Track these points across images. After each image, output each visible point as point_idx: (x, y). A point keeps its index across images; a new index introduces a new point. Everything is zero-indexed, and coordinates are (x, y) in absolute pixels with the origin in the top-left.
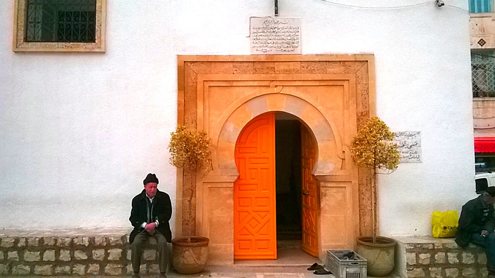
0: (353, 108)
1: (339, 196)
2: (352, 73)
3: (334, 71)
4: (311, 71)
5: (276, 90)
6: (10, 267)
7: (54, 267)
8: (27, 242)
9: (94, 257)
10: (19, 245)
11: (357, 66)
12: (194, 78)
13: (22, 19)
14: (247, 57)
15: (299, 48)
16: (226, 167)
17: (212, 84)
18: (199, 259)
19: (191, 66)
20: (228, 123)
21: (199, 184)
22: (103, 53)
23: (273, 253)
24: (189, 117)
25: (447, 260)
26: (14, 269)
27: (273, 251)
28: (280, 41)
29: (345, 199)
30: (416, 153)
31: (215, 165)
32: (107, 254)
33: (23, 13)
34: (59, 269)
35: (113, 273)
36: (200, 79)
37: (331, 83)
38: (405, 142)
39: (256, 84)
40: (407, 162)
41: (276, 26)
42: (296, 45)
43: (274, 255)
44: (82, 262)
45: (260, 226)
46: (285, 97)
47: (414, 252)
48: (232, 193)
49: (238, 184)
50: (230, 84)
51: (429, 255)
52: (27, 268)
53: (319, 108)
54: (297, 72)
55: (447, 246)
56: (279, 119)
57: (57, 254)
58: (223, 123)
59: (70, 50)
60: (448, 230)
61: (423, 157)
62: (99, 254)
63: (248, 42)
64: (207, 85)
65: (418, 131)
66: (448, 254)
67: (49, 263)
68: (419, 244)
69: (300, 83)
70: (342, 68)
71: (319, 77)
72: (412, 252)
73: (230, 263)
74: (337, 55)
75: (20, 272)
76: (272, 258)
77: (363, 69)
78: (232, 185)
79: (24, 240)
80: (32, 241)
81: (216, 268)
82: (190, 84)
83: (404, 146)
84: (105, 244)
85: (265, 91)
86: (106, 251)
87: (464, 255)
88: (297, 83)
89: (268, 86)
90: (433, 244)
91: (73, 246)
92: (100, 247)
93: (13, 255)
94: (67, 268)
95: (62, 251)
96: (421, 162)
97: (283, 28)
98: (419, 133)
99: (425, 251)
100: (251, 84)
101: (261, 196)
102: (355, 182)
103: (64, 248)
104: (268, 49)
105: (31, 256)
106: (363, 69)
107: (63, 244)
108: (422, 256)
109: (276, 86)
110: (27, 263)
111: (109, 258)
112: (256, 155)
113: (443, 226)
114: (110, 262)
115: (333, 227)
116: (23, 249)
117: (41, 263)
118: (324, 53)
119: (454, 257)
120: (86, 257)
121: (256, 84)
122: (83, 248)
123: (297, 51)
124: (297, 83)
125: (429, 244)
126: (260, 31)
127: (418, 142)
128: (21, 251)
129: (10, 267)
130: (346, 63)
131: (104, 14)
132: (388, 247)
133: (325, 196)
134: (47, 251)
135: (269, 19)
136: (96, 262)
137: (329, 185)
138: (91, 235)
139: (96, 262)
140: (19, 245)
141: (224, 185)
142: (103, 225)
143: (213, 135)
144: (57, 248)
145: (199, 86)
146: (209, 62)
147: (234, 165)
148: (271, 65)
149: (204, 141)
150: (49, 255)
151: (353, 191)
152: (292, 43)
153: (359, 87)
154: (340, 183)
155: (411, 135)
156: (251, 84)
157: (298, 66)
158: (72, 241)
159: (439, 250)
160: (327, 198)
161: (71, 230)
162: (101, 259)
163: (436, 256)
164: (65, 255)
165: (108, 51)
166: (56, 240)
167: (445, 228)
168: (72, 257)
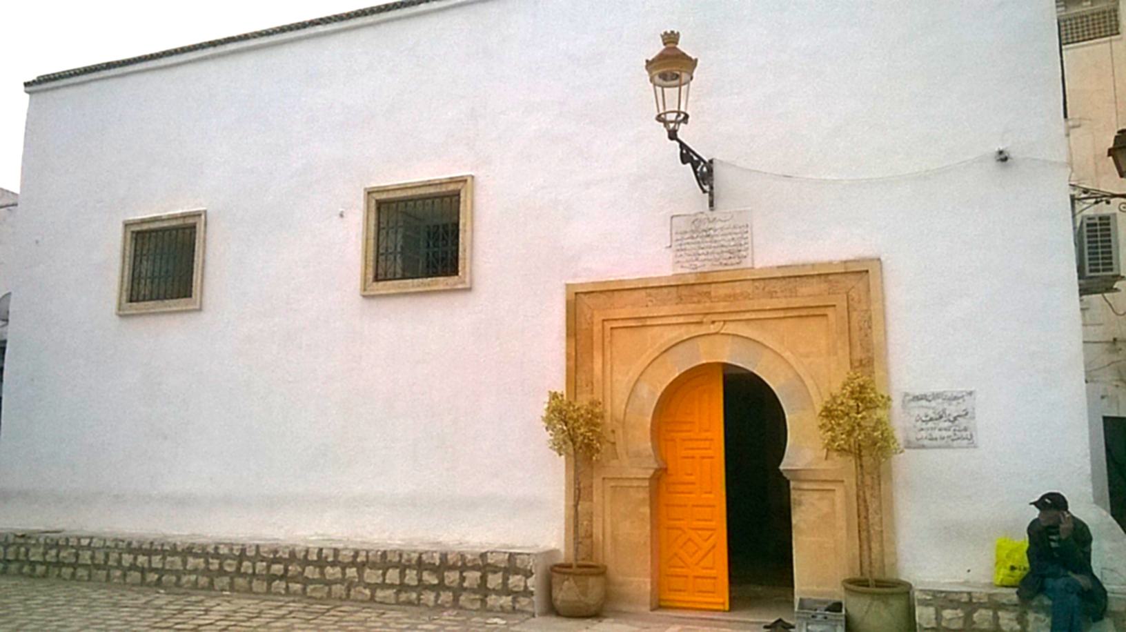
0: (843, 353)
1: (824, 506)
2: (844, 296)
3: (808, 293)
4: (771, 295)
5: (713, 328)
6: (349, 590)
7: (398, 592)
8: (367, 556)
9: (446, 582)
10: (359, 560)
11: (851, 281)
12: (590, 315)
13: (373, 222)
14: (667, 278)
15: (749, 260)
16: (638, 455)
17: (615, 324)
18: (584, 594)
19: (585, 298)
20: (639, 385)
21: (597, 482)
22: (469, 289)
23: (721, 600)
24: (582, 377)
25: (998, 625)
26: (352, 593)
27: (723, 597)
28: (719, 250)
29: (834, 512)
30: (965, 429)
31: (620, 449)
32: (463, 579)
33: (372, 242)
34: (403, 597)
35: (469, 606)
36: (598, 318)
37: (804, 313)
38: (944, 410)
39: (681, 320)
40: (949, 447)
41: (711, 226)
42: (744, 253)
43: (723, 604)
44: (432, 587)
45: (701, 553)
46: (730, 339)
47: (931, 605)
48: (647, 496)
49: (659, 478)
50: (641, 323)
51: (960, 613)
52: (367, 592)
53: (787, 354)
54: (747, 296)
55: (997, 598)
56: (729, 372)
57: (402, 575)
58: (633, 384)
59: (428, 288)
60: (1017, 572)
61: (980, 438)
62: (452, 577)
63: (670, 256)
64: (608, 325)
65: (969, 390)
66: (1000, 613)
67: (392, 586)
68: (942, 592)
69: (753, 316)
70: (824, 286)
71: (783, 303)
72: (927, 605)
73: (646, 609)
74: (813, 265)
75: (360, 597)
76: (721, 607)
77: (861, 285)
78: (647, 483)
79: (364, 553)
80: (375, 555)
81: (618, 614)
82: (585, 326)
83: (941, 417)
84: (460, 564)
85: (695, 331)
86: (461, 573)
87: (1031, 616)
88: (747, 316)
89: (700, 323)
90: (969, 593)
91: (420, 565)
92: (453, 568)
93: (351, 572)
94: (414, 596)
95: (407, 572)
96: (975, 447)
97: (722, 229)
98: (970, 393)
99: (955, 604)
100: (674, 320)
101: (701, 503)
102: (851, 481)
103: (409, 567)
104: (698, 264)
105: (372, 576)
106: (861, 285)
107: (409, 560)
108: (948, 614)
109: (713, 322)
110: (368, 585)
111: (465, 585)
112: (692, 435)
113: (1010, 564)
114: (465, 589)
115: (819, 556)
116: (364, 564)
117: (384, 586)
118: (789, 263)
119: (1011, 620)
120: (436, 582)
121: (681, 320)
122: (434, 569)
123: (747, 263)
124: (747, 316)
125: (962, 592)
126: (687, 236)
127: (970, 410)
128: (361, 567)
129: (349, 590)
130: (831, 278)
131: (468, 234)
132: (886, 594)
133: (800, 504)
134: (391, 571)
135: (700, 216)
136: (448, 588)
137: (805, 486)
138: (444, 550)
139: (448, 588)
140: (359, 560)
141: (635, 483)
142: (468, 538)
143: (615, 405)
144: (403, 568)
145: (597, 328)
146: (610, 291)
147: (651, 451)
148: (705, 289)
149: (595, 416)
150: (393, 576)
151: (847, 496)
152: (736, 252)
153: (854, 315)
154: (825, 484)
155: (956, 398)
156: (674, 320)
157: (748, 288)
158: (420, 558)
159: (981, 605)
160: (803, 508)
161: (423, 543)
162: (455, 584)
163: (975, 615)
164: (411, 577)
165: (476, 286)
166: (401, 555)
167: (1013, 568)
168: (420, 580)
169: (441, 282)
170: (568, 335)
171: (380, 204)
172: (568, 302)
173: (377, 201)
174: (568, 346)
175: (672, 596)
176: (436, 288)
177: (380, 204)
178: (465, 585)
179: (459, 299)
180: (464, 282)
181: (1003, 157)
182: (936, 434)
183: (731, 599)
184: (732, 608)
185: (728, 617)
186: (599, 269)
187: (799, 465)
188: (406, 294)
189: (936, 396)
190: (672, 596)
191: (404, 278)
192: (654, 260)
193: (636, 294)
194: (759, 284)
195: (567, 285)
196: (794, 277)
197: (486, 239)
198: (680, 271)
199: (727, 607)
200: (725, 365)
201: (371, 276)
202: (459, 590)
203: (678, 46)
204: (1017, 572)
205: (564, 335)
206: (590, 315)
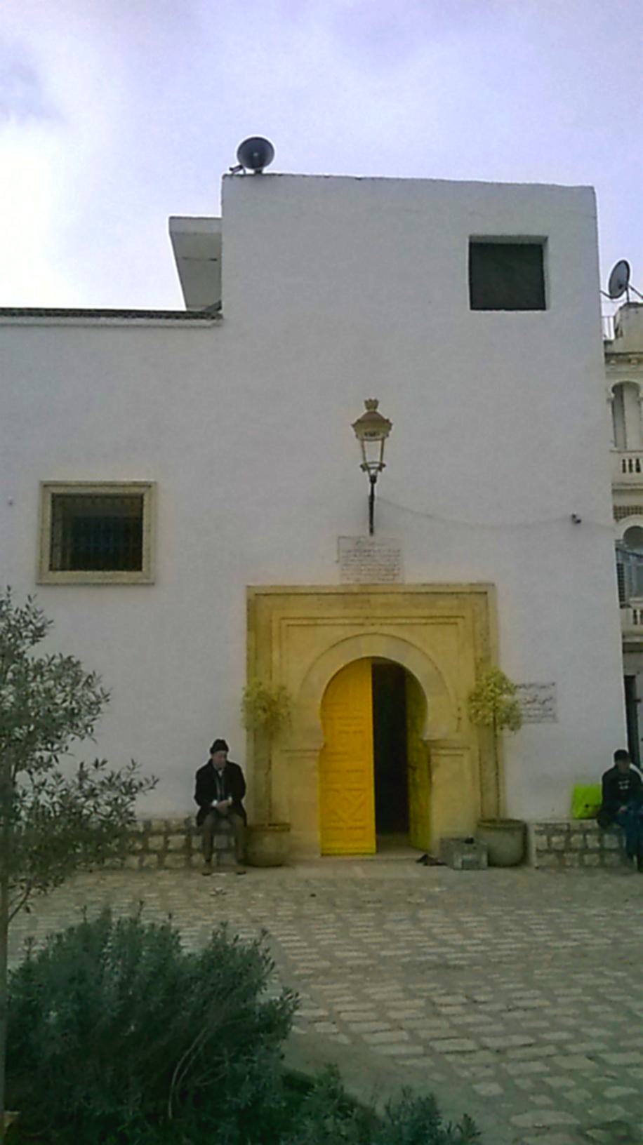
3: (445, 606)
12: (265, 613)
17: (292, 622)
22: (153, 584)
27: (370, 843)
32: (167, 842)
50: (312, 623)
51: (562, 838)
60: (590, 809)
64: (285, 622)
71: (426, 612)
73: (318, 856)
88: (399, 621)
89: (362, 625)
92: (158, 833)
100: (341, 621)
108: (554, 839)
114: (170, 851)
123: (399, 580)
124: (399, 621)
137: (443, 752)
138: (147, 817)
145: (275, 625)
159: (575, 832)
169: (125, 576)
170: (249, 630)
171: (55, 497)
172: (249, 601)
173: (53, 495)
174: (248, 638)
175: (334, 845)
176: (118, 581)
177: (55, 497)
178: (171, 847)
179: (142, 592)
180: (148, 578)
181: (576, 521)
182: (531, 713)
183: (378, 843)
184: (381, 846)
185: (375, 857)
186: (276, 575)
187: (436, 735)
188: (87, 584)
189: (531, 685)
190: (334, 845)
191: (63, 569)
192: (323, 571)
193: (309, 597)
194: (407, 596)
195: (249, 587)
196: (435, 593)
197: (165, 536)
198: (345, 581)
199: (374, 850)
200: (373, 658)
201: (46, 565)
202: (164, 852)
203: (378, 410)
204: (590, 809)
205: (245, 626)
206: (265, 613)
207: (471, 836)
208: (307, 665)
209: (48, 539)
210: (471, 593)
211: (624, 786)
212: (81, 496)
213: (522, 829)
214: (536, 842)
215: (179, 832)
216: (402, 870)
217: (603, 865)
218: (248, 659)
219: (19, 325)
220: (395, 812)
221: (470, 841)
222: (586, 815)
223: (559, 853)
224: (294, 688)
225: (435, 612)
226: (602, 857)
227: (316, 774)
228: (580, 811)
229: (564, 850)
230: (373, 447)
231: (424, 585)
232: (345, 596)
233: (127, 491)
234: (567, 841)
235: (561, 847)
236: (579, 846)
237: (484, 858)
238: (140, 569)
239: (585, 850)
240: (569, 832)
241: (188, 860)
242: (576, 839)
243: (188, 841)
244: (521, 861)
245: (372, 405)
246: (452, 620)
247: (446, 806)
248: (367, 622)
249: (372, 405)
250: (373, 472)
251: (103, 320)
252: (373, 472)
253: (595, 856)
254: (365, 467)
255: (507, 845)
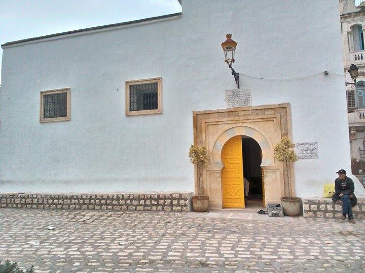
17: (209, 124)
22: (161, 113)
32: (165, 202)
50: (217, 124)
51: (316, 206)
60: (331, 194)
64: (207, 124)
73: (221, 209)
88: (250, 121)
92: (162, 199)
108: (313, 206)
114: (166, 205)
123: (250, 105)
124: (250, 121)
145: (203, 125)
170: (194, 127)
177: (131, 86)
179: (158, 117)
181: (326, 73)
185: (245, 210)
189: (306, 144)
193: (215, 114)
196: (264, 109)
200: (243, 136)
207: (278, 203)
208: (215, 141)
209: (129, 102)
210: (280, 108)
211: (344, 185)
212: (145, 85)
213: (299, 201)
214: (305, 207)
215: (168, 199)
216: (251, 215)
217: (334, 217)
218: (194, 137)
219: (104, 31)
220: (254, 191)
221: (279, 206)
222: (329, 196)
223: (315, 212)
224: (210, 148)
225: (265, 117)
226: (334, 214)
227: (220, 179)
228: (327, 194)
229: (317, 210)
230: (229, 53)
231: (259, 106)
232: (229, 113)
233: (135, 84)
234: (318, 207)
235: (316, 209)
236: (323, 209)
237: (281, 212)
238: (157, 108)
239: (326, 211)
240: (319, 204)
241: (172, 208)
242: (322, 207)
243: (172, 202)
244: (300, 214)
245: (229, 36)
246: (272, 119)
247: (272, 191)
248: (237, 122)
249: (229, 36)
250: (230, 63)
251: (143, 23)
252: (230, 63)
253: (331, 213)
254: (226, 61)
255: (291, 208)
